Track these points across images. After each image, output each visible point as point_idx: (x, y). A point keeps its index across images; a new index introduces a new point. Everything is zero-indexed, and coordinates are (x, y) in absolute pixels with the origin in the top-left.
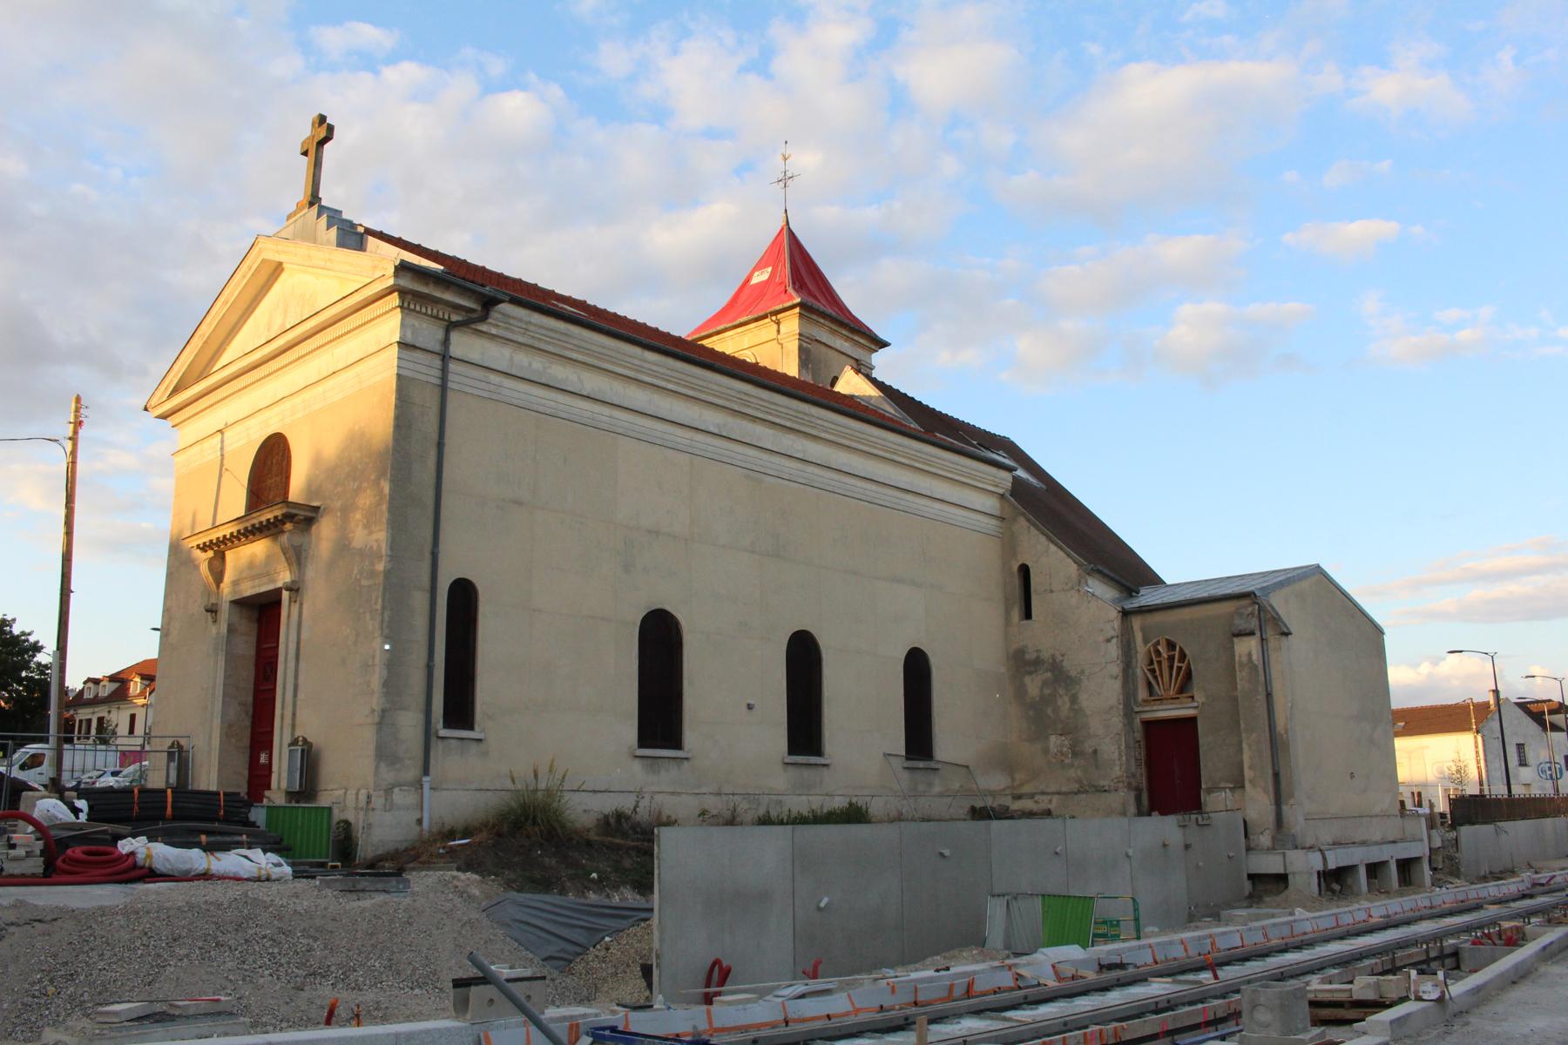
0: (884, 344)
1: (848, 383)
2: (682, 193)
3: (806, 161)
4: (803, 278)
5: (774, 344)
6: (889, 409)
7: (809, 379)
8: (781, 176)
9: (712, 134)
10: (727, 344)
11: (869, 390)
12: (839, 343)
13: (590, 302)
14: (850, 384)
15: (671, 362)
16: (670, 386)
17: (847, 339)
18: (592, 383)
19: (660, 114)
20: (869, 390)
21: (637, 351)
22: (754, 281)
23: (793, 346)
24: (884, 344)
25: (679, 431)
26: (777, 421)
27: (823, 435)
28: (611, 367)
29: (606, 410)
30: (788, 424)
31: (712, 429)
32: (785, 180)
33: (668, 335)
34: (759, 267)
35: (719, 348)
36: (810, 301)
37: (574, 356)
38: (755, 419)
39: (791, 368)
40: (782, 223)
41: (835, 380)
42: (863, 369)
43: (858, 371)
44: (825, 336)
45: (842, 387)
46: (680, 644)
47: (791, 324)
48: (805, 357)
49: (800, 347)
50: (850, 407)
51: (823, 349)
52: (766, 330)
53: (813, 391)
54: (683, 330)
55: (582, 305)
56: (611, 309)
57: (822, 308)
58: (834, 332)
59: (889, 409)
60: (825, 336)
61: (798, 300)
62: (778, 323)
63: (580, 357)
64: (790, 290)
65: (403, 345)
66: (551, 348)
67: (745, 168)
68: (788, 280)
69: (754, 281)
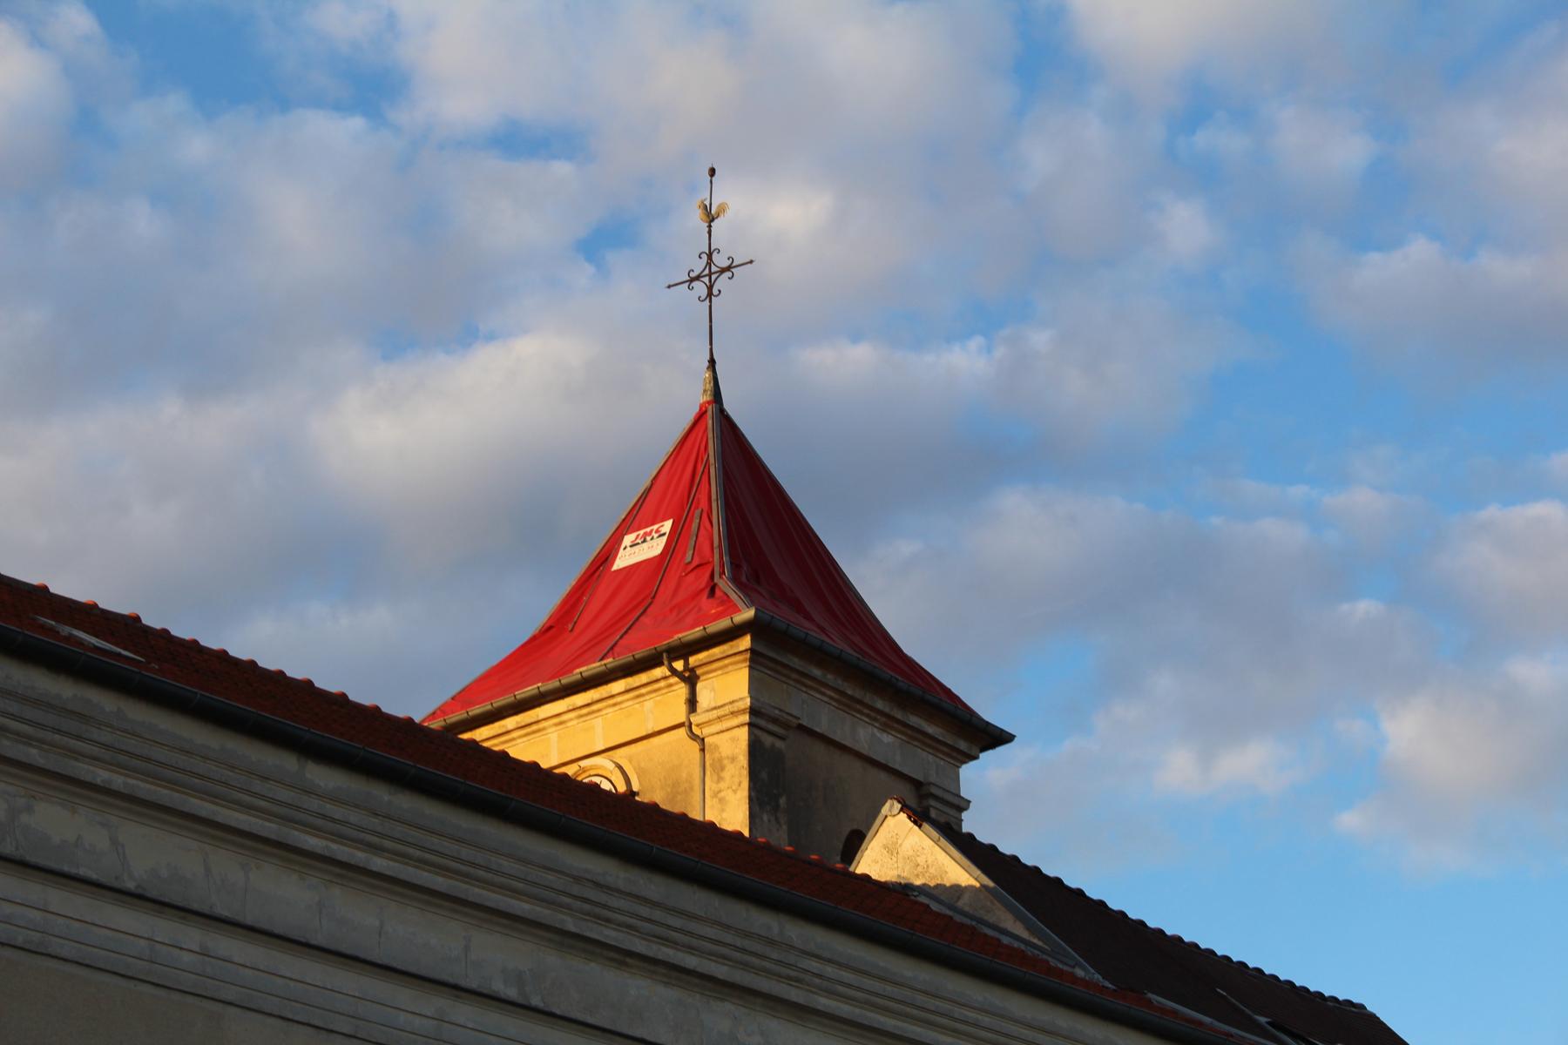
0: (996, 738)
1: (892, 849)
2: (427, 305)
3: (780, 216)
4: (749, 544)
5: (671, 739)
6: (1012, 924)
7: (780, 839)
8: (699, 266)
9: (518, 141)
10: (550, 739)
11: (954, 871)
12: (867, 736)
13: (151, 620)
14: (898, 851)
15: (383, 794)
16: (379, 863)
17: (889, 723)
18: (150, 854)
19: (372, 86)
20: (954, 871)
21: (285, 762)
22: (625, 558)
23: (734, 744)
24: (996, 738)
25: (404, 995)
26: (691, 961)
27: (824, 1003)
28: (205, 808)
29: (193, 935)
30: (720, 971)
31: (499, 987)
32: (711, 274)
33: (373, 715)
34: (635, 519)
35: (522, 750)
36: (784, 616)
37: (101, 775)
38: (623, 958)
39: (730, 809)
40: (694, 397)
41: (854, 842)
42: (938, 812)
43: (919, 817)
44: (825, 717)
45: (874, 863)
46: (1373, 1020)
47: (728, 684)
48: (768, 775)
49: (755, 749)
50: (900, 915)
51: (819, 750)
52: (652, 703)
53: (790, 870)
54: (416, 702)
55: (127, 628)
56: (210, 641)
57: (815, 635)
58: (849, 704)
59: (1012, 924)
60: (825, 717)
61: (748, 614)
62: (691, 678)
63: (118, 781)
64: (725, 585)
65: (753, 711)
66: (34, 755)
67: (607, 239)
68: (718, 557)
69: (625, 558)
